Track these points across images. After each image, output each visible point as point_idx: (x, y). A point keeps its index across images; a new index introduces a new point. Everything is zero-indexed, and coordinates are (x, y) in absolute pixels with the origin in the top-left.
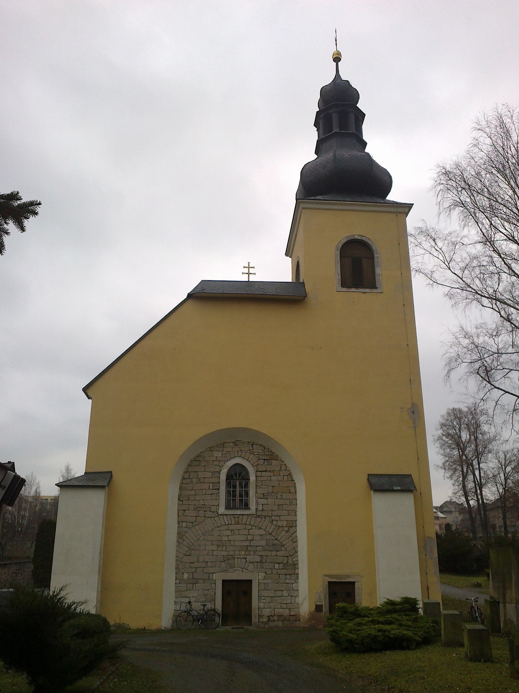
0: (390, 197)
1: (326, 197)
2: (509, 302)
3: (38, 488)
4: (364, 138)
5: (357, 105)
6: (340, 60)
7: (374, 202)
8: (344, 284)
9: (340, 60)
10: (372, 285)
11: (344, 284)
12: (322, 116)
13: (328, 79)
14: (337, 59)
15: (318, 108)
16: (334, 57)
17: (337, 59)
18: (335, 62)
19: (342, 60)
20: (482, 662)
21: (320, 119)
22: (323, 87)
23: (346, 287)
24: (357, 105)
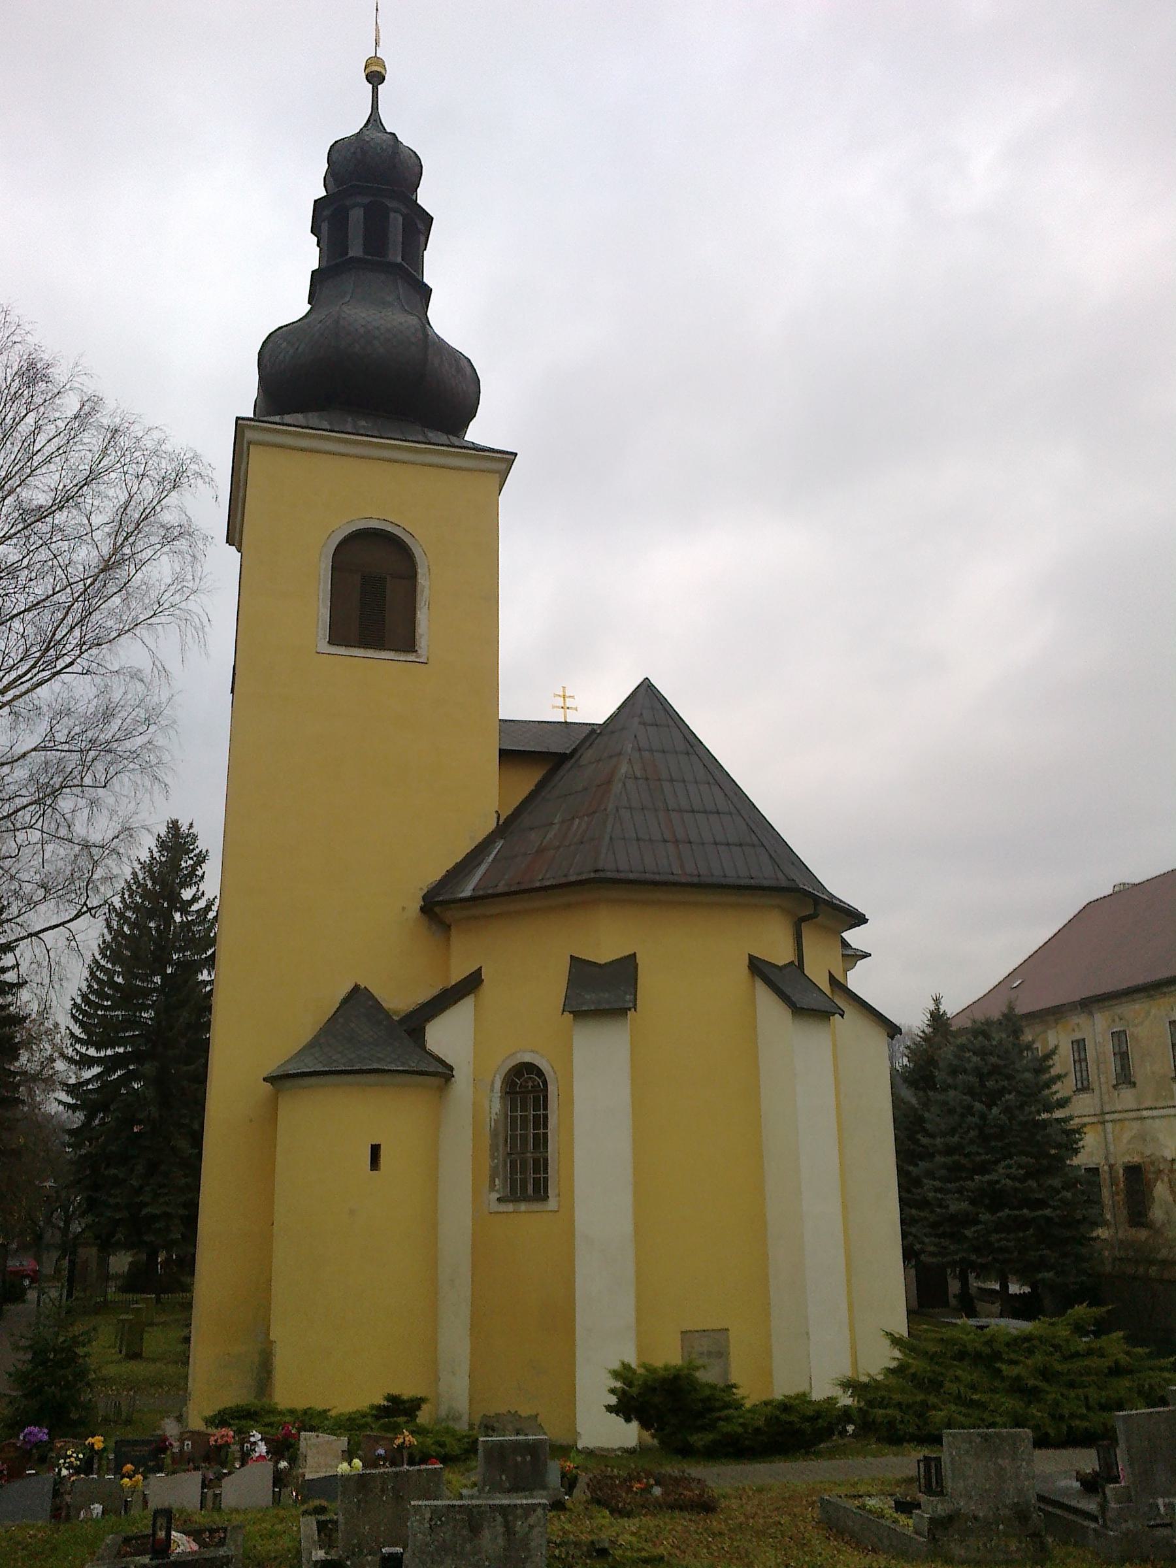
0: (476, 433)
1: (299, 418)
2: (64, 628)
3: (875, 1417)
4: (426, 280)
5: (325, 194)
6: (382, 79)
7: (424, 440)
8: (338, 637)
9: (384, 79)
10: (408, 644)
11: (338, 637)
12: (326, 213)
13: (352, 125)
14: (375, 78)
15: (324, 189)
16: (368, 70)
17: (375, 78)
18: (370, 83)
19: (386, 78)
20: (273, 1491)
21: (324, 221)
22: (336, 142)
23: (393, 650)
24: (325, 194)
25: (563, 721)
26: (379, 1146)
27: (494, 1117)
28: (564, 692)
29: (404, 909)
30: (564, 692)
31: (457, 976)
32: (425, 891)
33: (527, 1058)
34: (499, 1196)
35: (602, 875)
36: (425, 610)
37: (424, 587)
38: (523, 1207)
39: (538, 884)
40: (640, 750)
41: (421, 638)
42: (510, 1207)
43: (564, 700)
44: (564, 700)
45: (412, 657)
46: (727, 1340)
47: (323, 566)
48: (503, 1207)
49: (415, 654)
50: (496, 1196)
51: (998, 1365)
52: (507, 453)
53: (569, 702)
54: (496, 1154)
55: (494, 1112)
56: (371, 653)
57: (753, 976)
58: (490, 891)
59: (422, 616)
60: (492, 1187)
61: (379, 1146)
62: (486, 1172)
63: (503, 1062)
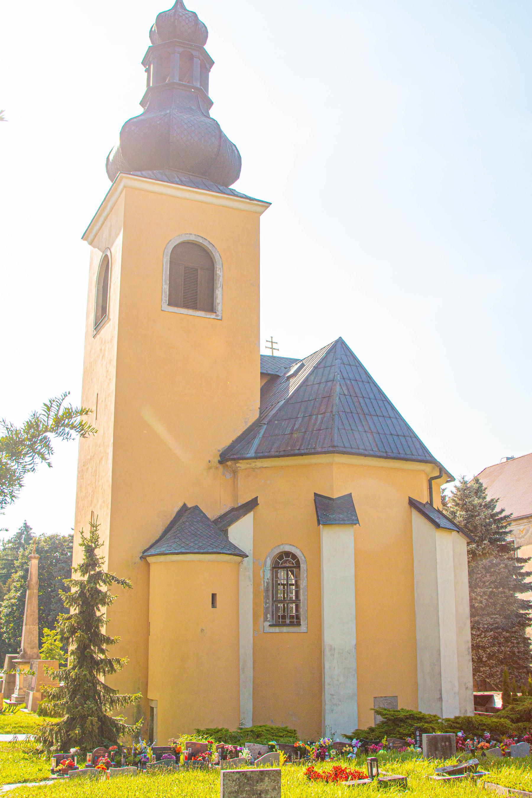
8: (172, 303)
25: (271, 355)
26: (215, 594)
27: (266, 580)
28: (272, 339)
29: (209, 462)
30: (272, 339)
31: (242, 501)
32: (221, 452)
33: (287, 548)
34: (270, 624)
35: (337, 449)
36: (220, 289)
37: (220, 276)
38: (285, 629)
39: (297, 452)
40: (344, 379)
41: (218, 305)
42: (277, 629)
43: (272, 344)
44: (272, 344)
45: (213, 316)
46: (397, 702)
47: (165, 260)
48: (273, 629)
49: (215, 314)
50: (268, 623)
51: (386, 736)
52: (267, 203)
53: (275, 346)
54: (268, 601)
55: (266, 578)
56: (191, 312)
57: (411, 508)
58: (266, 454)
59: (218, 293)
60: (266, 619)
61: (215, 594)
62: (262, 611)
63: (272, 550)
